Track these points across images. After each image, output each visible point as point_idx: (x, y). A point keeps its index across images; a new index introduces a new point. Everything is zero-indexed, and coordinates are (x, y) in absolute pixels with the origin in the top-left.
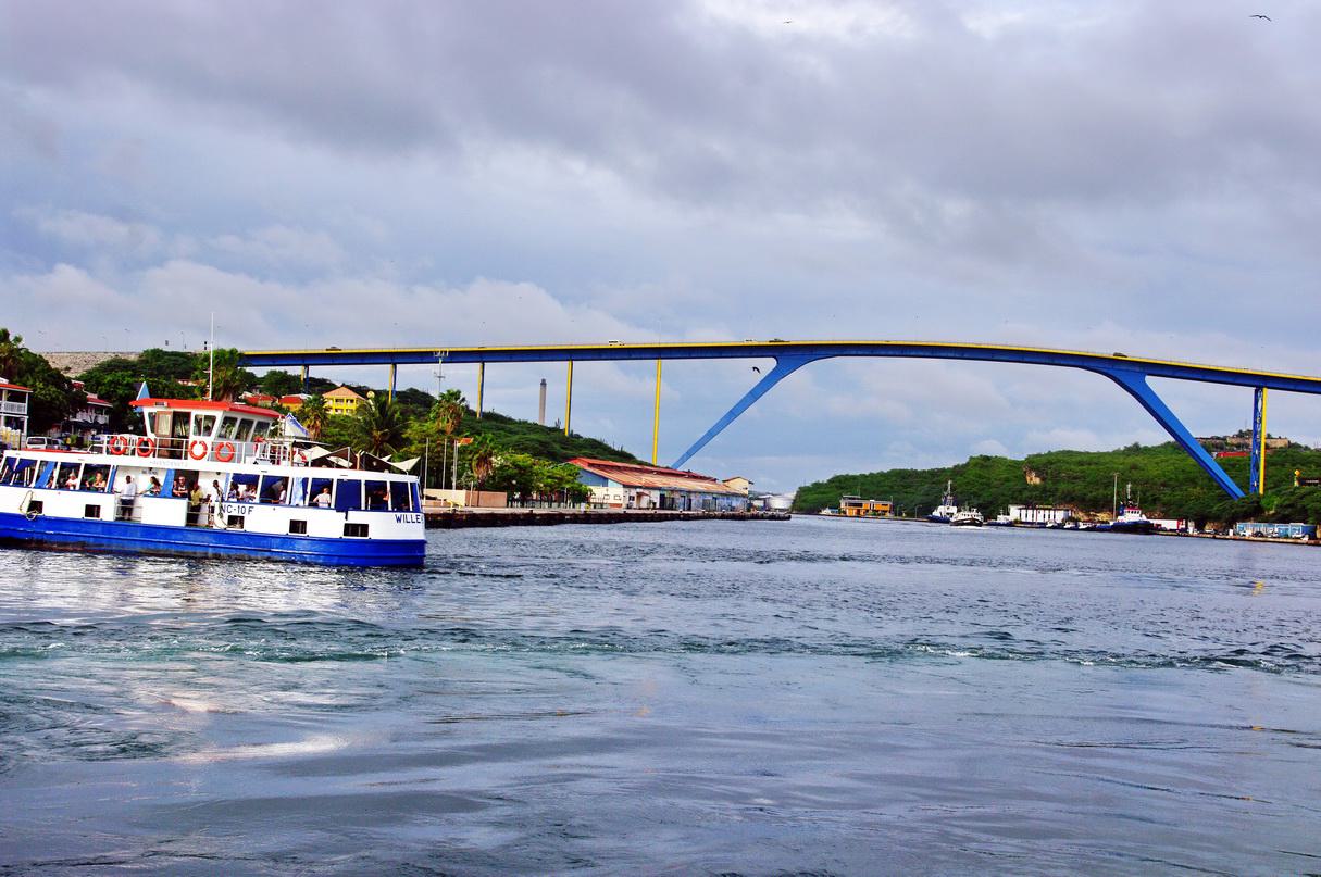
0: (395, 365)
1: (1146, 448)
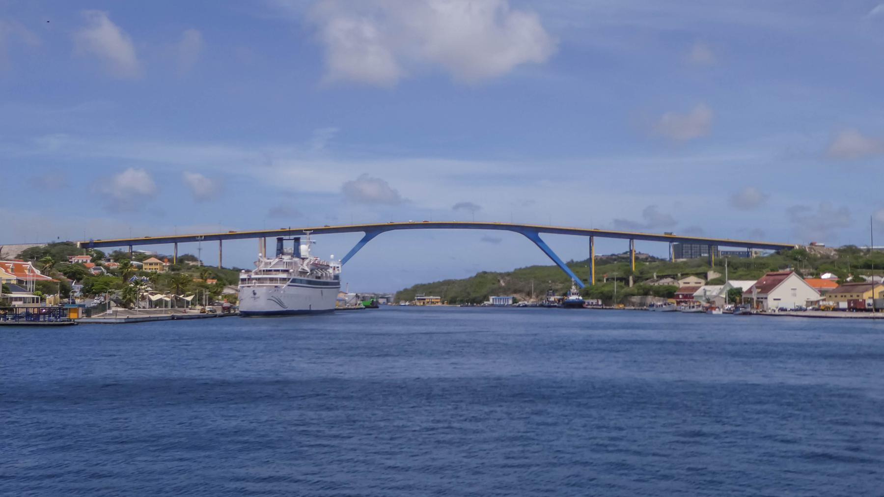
0: (221, 240)
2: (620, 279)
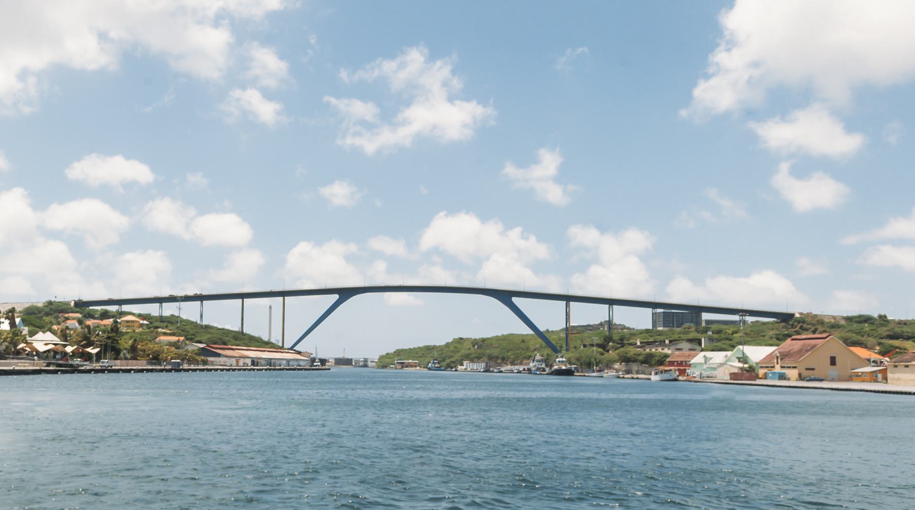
0: (202, 301)
1: (552, 331)
2: (599, 346)
